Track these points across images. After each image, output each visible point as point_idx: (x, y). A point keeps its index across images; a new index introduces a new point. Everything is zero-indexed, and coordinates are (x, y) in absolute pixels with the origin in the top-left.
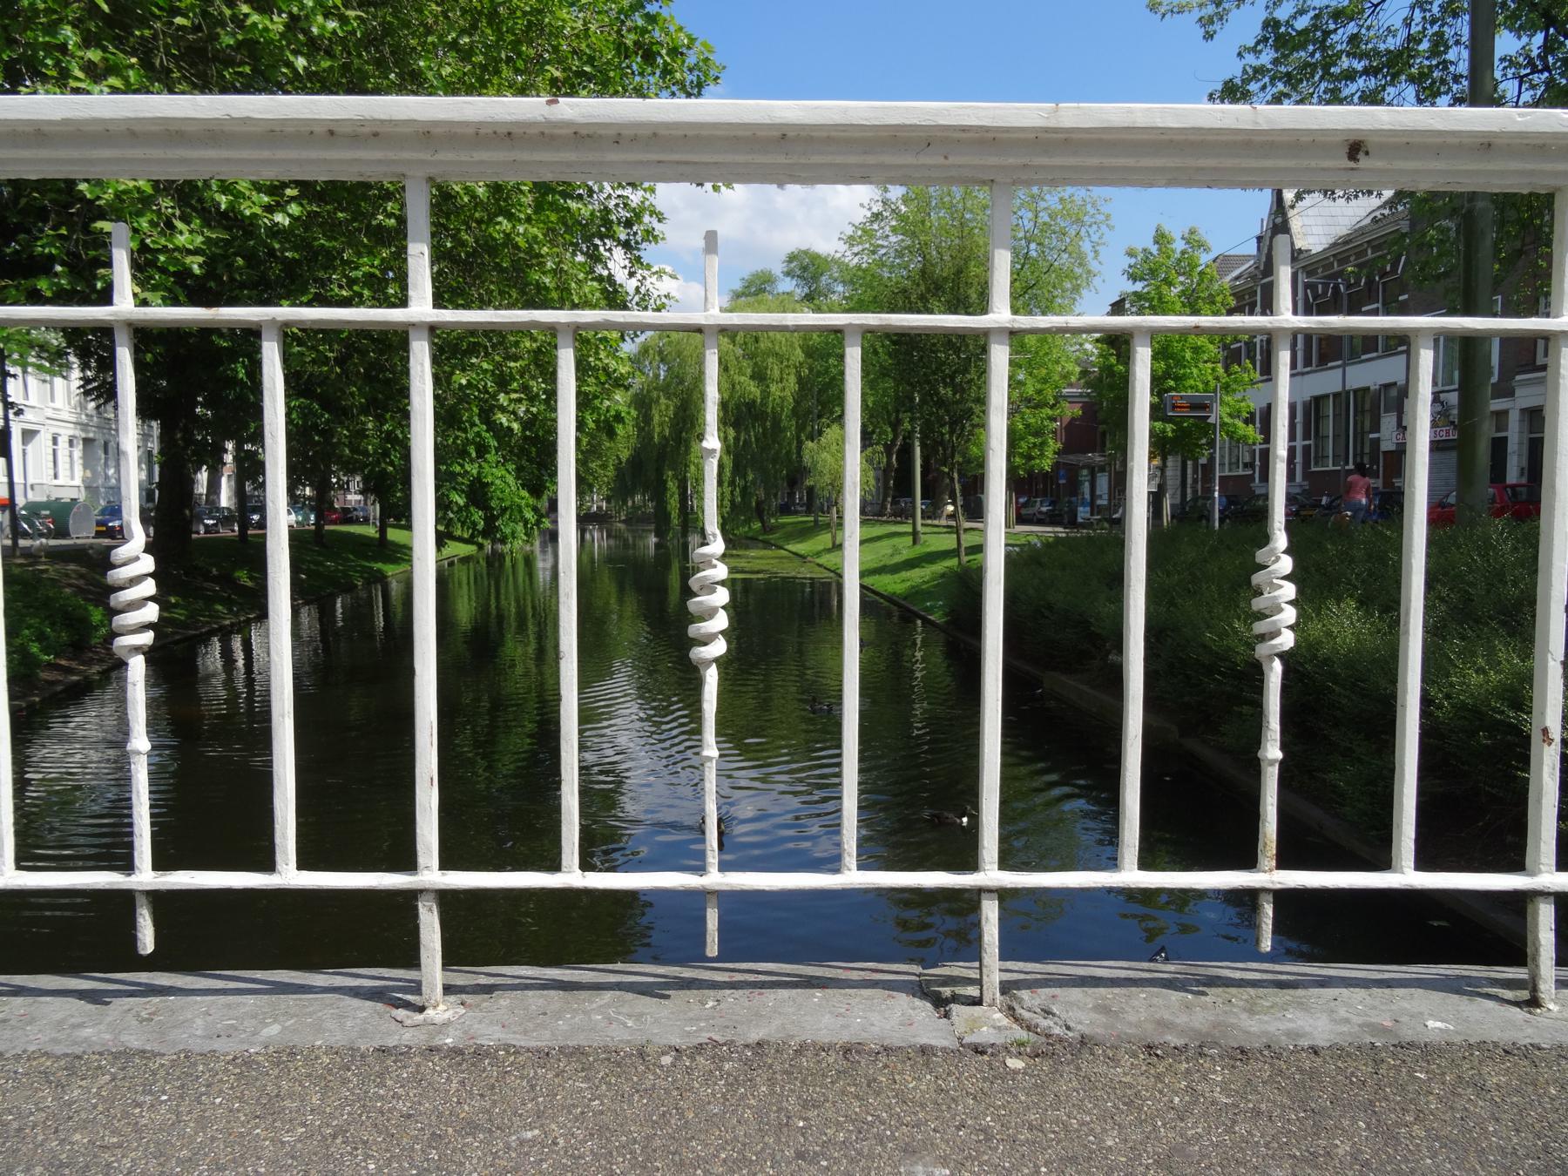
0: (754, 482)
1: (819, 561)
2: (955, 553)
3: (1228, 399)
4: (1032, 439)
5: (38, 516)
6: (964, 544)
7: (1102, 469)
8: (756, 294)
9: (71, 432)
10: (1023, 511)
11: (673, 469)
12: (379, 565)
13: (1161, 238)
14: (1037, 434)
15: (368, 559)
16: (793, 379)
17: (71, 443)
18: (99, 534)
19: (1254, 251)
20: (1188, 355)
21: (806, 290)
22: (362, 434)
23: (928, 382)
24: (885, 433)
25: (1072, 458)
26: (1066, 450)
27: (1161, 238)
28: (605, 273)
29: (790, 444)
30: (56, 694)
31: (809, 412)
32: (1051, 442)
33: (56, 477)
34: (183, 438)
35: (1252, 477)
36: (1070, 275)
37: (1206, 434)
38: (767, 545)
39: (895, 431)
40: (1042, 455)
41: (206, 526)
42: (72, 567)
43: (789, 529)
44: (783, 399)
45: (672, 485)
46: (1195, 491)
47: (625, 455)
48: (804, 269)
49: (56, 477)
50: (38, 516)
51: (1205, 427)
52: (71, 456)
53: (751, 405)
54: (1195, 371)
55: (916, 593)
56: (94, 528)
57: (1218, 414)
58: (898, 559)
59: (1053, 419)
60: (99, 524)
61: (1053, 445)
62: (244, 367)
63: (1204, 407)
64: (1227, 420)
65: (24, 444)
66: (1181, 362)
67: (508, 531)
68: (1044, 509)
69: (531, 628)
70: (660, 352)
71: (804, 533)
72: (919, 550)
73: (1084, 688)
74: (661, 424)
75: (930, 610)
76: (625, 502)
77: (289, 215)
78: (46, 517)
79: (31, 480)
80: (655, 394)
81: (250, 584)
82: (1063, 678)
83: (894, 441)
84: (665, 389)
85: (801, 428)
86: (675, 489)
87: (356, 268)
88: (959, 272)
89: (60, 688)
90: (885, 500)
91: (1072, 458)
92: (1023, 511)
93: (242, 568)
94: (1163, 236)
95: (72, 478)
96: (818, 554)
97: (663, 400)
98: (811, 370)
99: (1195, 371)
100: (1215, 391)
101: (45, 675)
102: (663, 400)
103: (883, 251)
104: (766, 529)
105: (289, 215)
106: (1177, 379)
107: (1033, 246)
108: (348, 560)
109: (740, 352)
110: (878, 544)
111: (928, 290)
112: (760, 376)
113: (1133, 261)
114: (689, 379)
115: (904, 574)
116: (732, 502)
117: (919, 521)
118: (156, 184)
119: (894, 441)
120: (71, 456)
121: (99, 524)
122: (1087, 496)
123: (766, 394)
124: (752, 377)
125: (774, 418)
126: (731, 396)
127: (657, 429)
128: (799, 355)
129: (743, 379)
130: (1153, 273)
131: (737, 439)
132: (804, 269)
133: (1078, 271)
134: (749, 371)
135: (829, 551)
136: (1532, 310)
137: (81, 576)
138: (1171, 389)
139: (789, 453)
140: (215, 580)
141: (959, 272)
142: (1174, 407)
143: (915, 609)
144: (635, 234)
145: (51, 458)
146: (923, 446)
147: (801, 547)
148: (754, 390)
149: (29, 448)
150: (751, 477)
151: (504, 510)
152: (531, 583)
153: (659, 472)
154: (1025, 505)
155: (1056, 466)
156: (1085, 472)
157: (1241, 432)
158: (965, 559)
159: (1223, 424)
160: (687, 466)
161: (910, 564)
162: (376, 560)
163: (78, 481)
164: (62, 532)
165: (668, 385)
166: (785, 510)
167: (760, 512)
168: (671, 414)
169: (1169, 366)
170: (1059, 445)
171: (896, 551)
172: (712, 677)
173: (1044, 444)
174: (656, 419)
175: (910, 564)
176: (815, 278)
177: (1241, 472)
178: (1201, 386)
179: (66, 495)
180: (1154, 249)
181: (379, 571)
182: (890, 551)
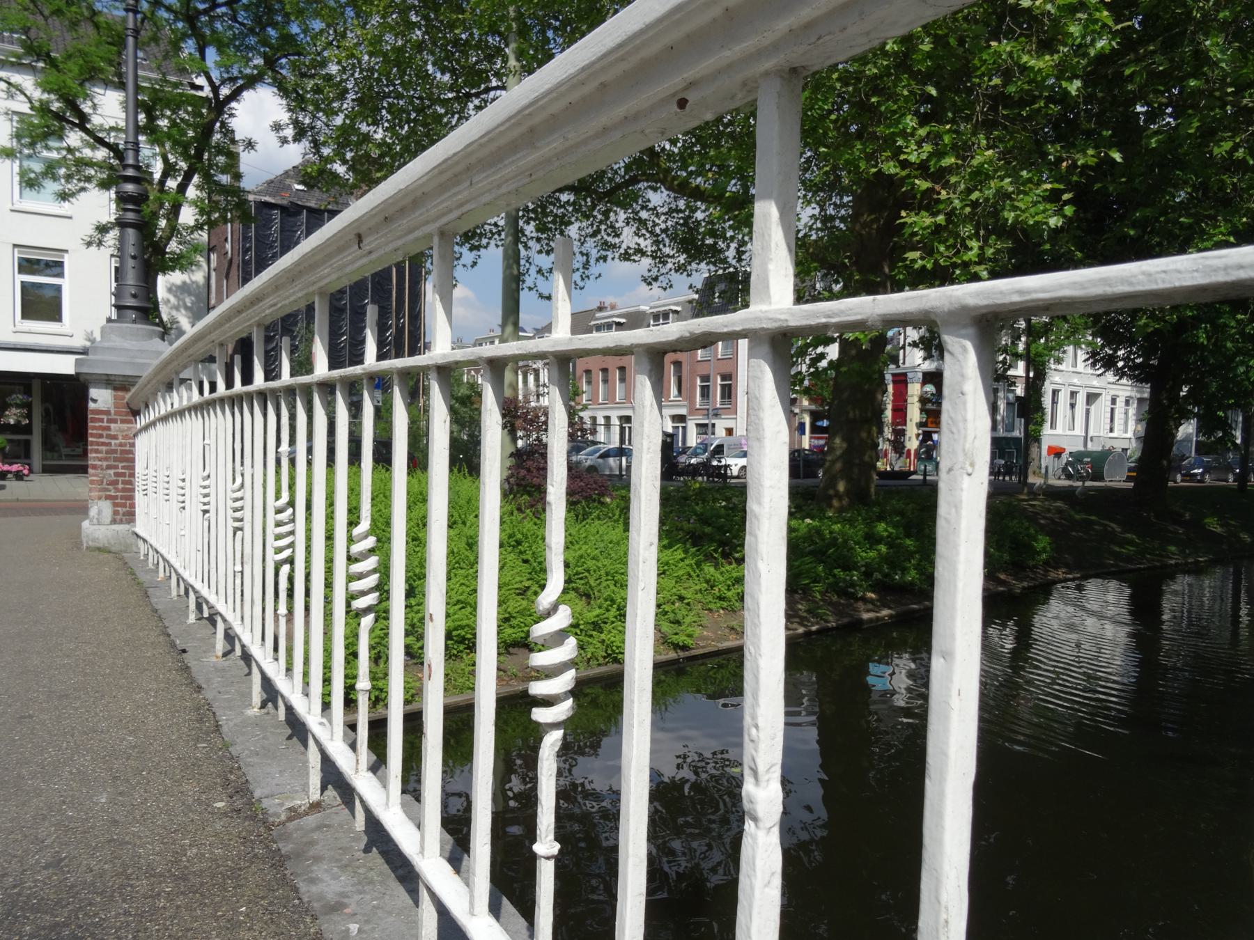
5: (1081, 462)
9: (1128, 394)
17: (1127, 403)
33: (1111, 430)
49: (1111, 430)
50: (1081, 462)
52: (1126, 413)
56: (1126, 473)
62: (1206, 332)
65: (1088, 403)
79: (1091, 433)
81: (1219, 530)
95: (1126, 432)
118: (40, 185)
120: (1126, 413)
136: (414, 351)
145: (1109, 415)
149: (1093, 408)
163: (1130, 434)
164: (1098, 476)
172: (552, 742)
179: (1119, 445)
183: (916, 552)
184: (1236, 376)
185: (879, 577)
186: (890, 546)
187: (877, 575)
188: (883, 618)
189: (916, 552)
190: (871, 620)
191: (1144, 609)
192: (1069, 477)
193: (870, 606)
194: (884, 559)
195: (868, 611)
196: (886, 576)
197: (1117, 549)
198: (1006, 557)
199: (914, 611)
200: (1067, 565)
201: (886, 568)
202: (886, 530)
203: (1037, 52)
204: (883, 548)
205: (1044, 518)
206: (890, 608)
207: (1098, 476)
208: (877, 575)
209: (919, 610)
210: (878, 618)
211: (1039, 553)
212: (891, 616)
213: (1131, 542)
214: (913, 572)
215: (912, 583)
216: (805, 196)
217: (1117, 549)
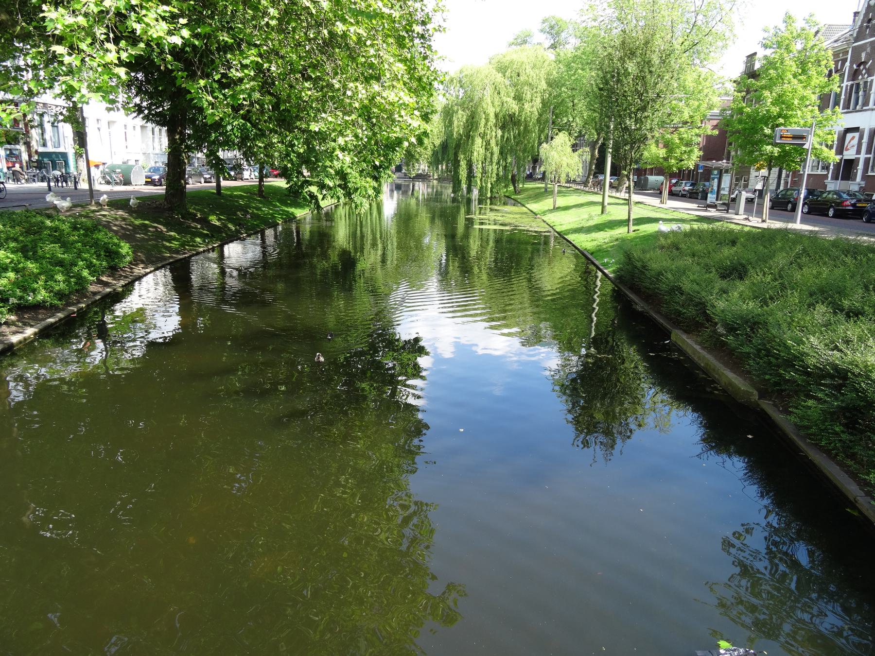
0: (511, 164)
1: (545, 218)
2: (626, 223)
3: (819, 132)
4: (684, 148)
6: (633, 217)
7: (727, 171)
8: (520, 44)
10: (674, 189)
11: (465, 154)
12: (292, 210)
13: (788, 19)
14: (687, 145)
15: (287, 205)
16: (539, 100)
18: (147, 183)
19: (851, 22)
20: (796, 102)
21: (552, 42)
22: (271, 145)
23: (620, 116)
24: (593, 134)
25: (709, 164)
26: (704, 158)
27: (788, 19)
28: (409, 56)
29: (534, 141)
30: (96, 301)
31: (547, 121)
32: (696, 150)
34: (180, 138)
35: (826, 176)
36: (723, 38)
37: (801, 154)
38: (516, 203)
39: (598, 134)
40: (689, 158)
41: (205, 179)
42: (120, 213)
43: (531, 192)
44: (532, 113)
45: (463, 164)
46: (786, 183)
47: (438, 142)
48: (552, 28)
51: (800, 150)
53: (512, 116)
54: (799, 113)
55: (600, 251)
56: (145, 180)
57: (811, 142)
58: (592, 223)
59: (698, 135)
60: (147, 177)
61: (697, 153)
63: (802, 137)
64: (817, 146)
66: (789, 107)
67: (359, 202)
68: (687, 188)
69: (380, 246)
70: (460, 81)
71: (538, 196)
72: (605, 218)
73: (697, 347)
74: (458, 127)
75: (606, 265)
76: (437, 168)
77: (182, 38)
78: (119, 173)
80: (456, 108)
81: (218, 223)
82: (684, 337)
83: (598, 139)
84: (462, 105)
85: (541, 131)
86: (464, 166)
87: (246, 58)
88: (647, 43)
89: (98, 297)
90: (588, 177)
91: (709, 164)
92: (674, 189)
93: (214, 214)
94: (790, 18)
96: (544, 213)
97: (460, 112)
98: (550, 95)
99: (799, 113)
100: (811, 126)
101: (92, 288)
102: (460, 112)
103: (602, 19)
104: (516, 192)
105: (182, 38)
106: (786, 117)
107: (700, 17)
108: (275, 206)
109: (507, 83)
110: (582, 210)
111: (626, 55)
112: (518, 98)
113: (766, 35)
114: (476, 99)
115: (594, 235)
116: (497, 175)
117: (607, 193)
119: (597, 141)
121: (147, 177)
122: (715, 188)
123: (521, 110)
124: (514, 99)
125: (526, 125)
126: (501, 110)
127: (456, 130)
128: (543, 85)
129: (508, 99)
130: (779, 45)
131: (503, 137)
132: (552, 28)
133: (727, 34)
134: (512, 95)
135: (550, 211)
137: (124, 219)
138: (782, 124)
139: (533, 146)
140: (199, 221)
141: (647, 43)
142: (782, 137)
143: (597, 262)
144: (428, 30)
146: (614, 157)
147: (534, 206)
148: (514, 107)
150: (509, 160)
151: (356, 190)
152: (380, 217)
153: (456, 155)
154: (675, 185)
155: (697, 166)
156: (716, 172)
157: (826, 155)
158: (632, 228)
159: (814, 148)
160: (472, 152)
161: (599, 228)
162: (291, 205)
165: (464, 103)
166: (530, 177)
167: (514, 181)
168: (464, 120)
169: (781, 109)
170: (701, 153)
171: (591, 217)
173: (691, 151)
174: (456, 123)
175: (599, 228)
176: (558, 34)
177: (819, 172)
178: (802, 122)
180: (782, 26)
181: (292, 214)
182: (586, 217)
183: (40, 274)
184: (227, 131)
185: (15, 301)
186: (16, 270)
187: (13, 300)
188: (29, 337)
189: (40, 274)
190: (20, 342)
191: (181, 282)
192: (108, 183)
193: (14, 328)
194: (16, 284)
195: (14, 333)
196: (21, 298)
197: (168, 244)
198: (104, 263)
199: (52, 324)
200: (143, 262)
201: (18, 292)
202: (8, 257)
203: (456, 342)
204: (12, 275)
205: (115, 225)
206: (32, 326)
207: (127, 183)
208: (13, 300)
209: (56, 322)
210: (25, 339)
211: (124, 257)
212: (35, 334)
213: (175, 239)
214: (43, 292)
215: (44, 302)
216: (95, 82)
217: (168, 244)
